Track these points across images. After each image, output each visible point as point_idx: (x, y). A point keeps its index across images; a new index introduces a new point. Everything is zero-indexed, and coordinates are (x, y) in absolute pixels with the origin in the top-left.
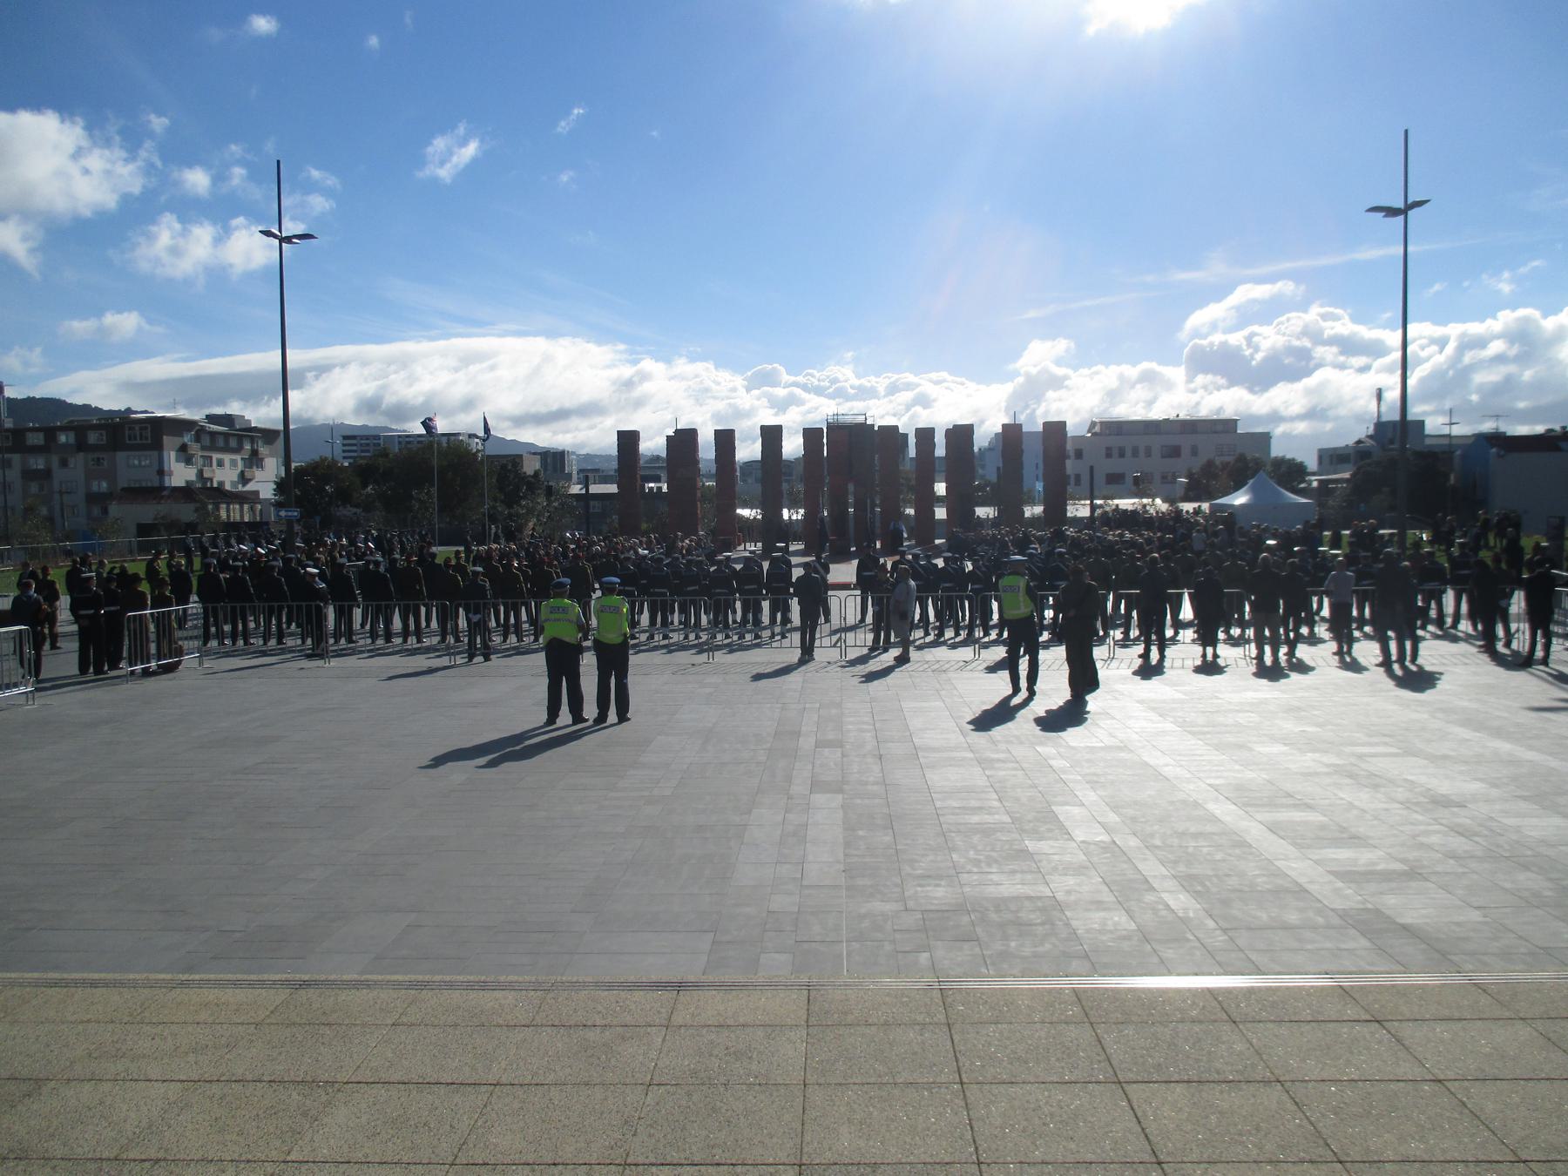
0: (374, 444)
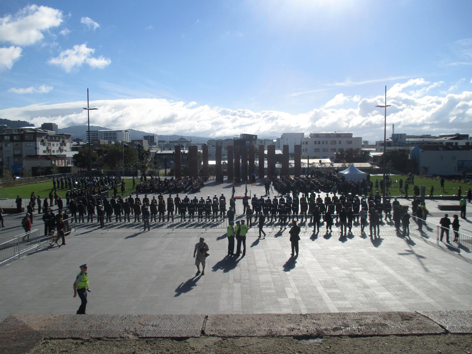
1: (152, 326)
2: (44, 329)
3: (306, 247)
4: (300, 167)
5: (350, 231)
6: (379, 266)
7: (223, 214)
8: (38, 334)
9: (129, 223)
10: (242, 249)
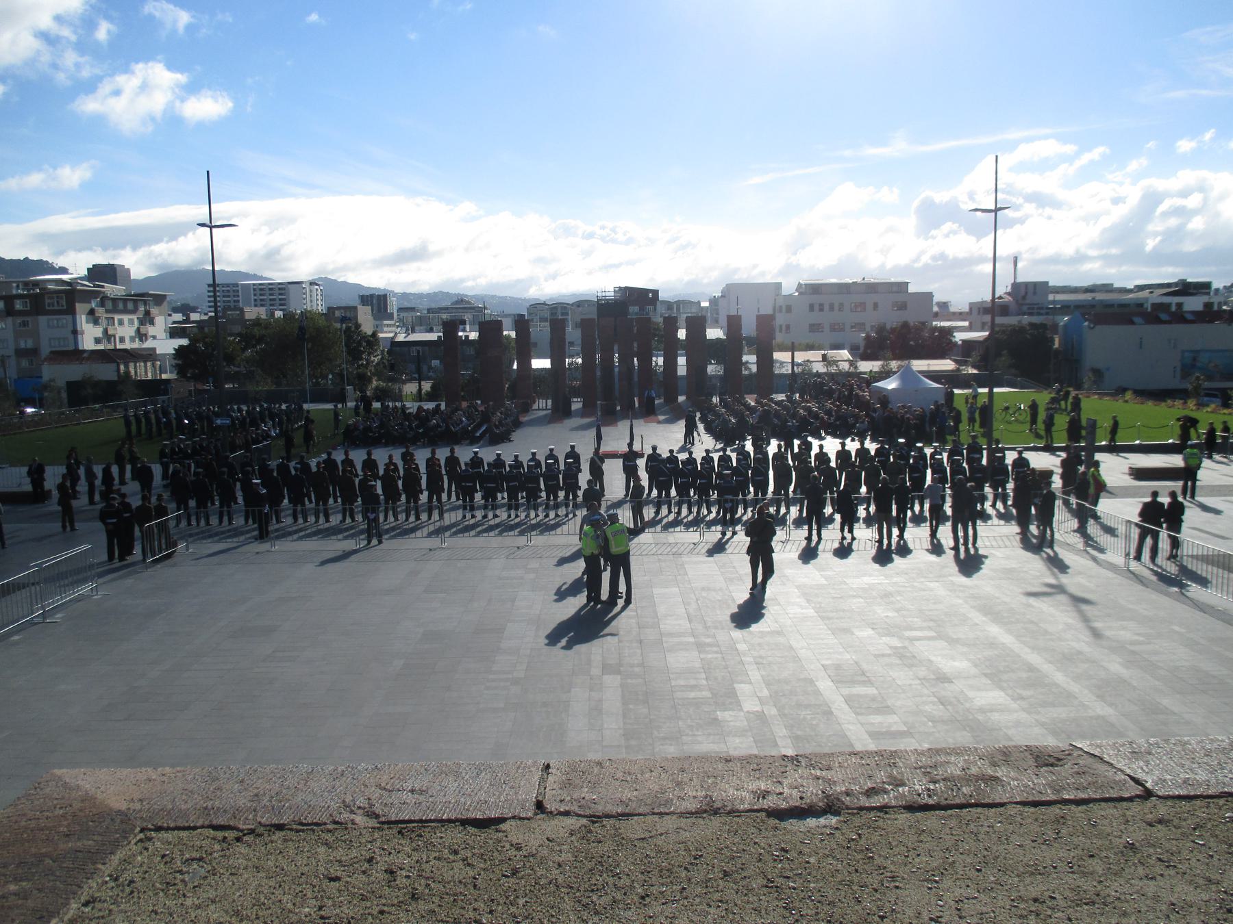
0: (234, 291)
1: (412, 791)
2: (138, 806)
3: (788, 580)
4: (772, 372)
5: (901, 536)
6: (977, 624)
7: (571, 497)
8: (125, 817)
9: (327, 525)
10: (622, 588)
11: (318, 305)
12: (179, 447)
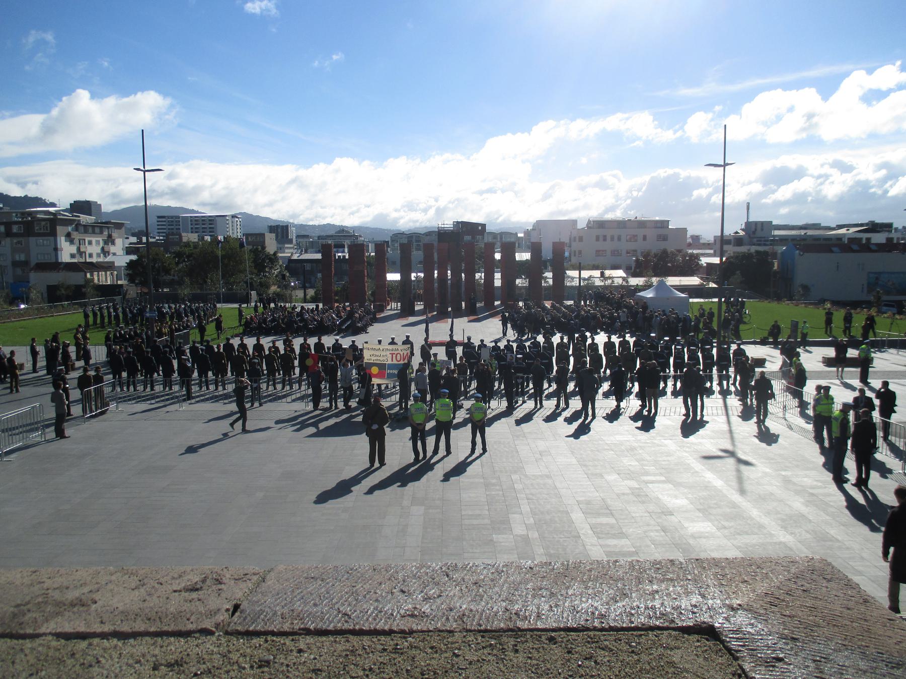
0: (176, 221)
11: (237, 232)
12: (120, 333)
